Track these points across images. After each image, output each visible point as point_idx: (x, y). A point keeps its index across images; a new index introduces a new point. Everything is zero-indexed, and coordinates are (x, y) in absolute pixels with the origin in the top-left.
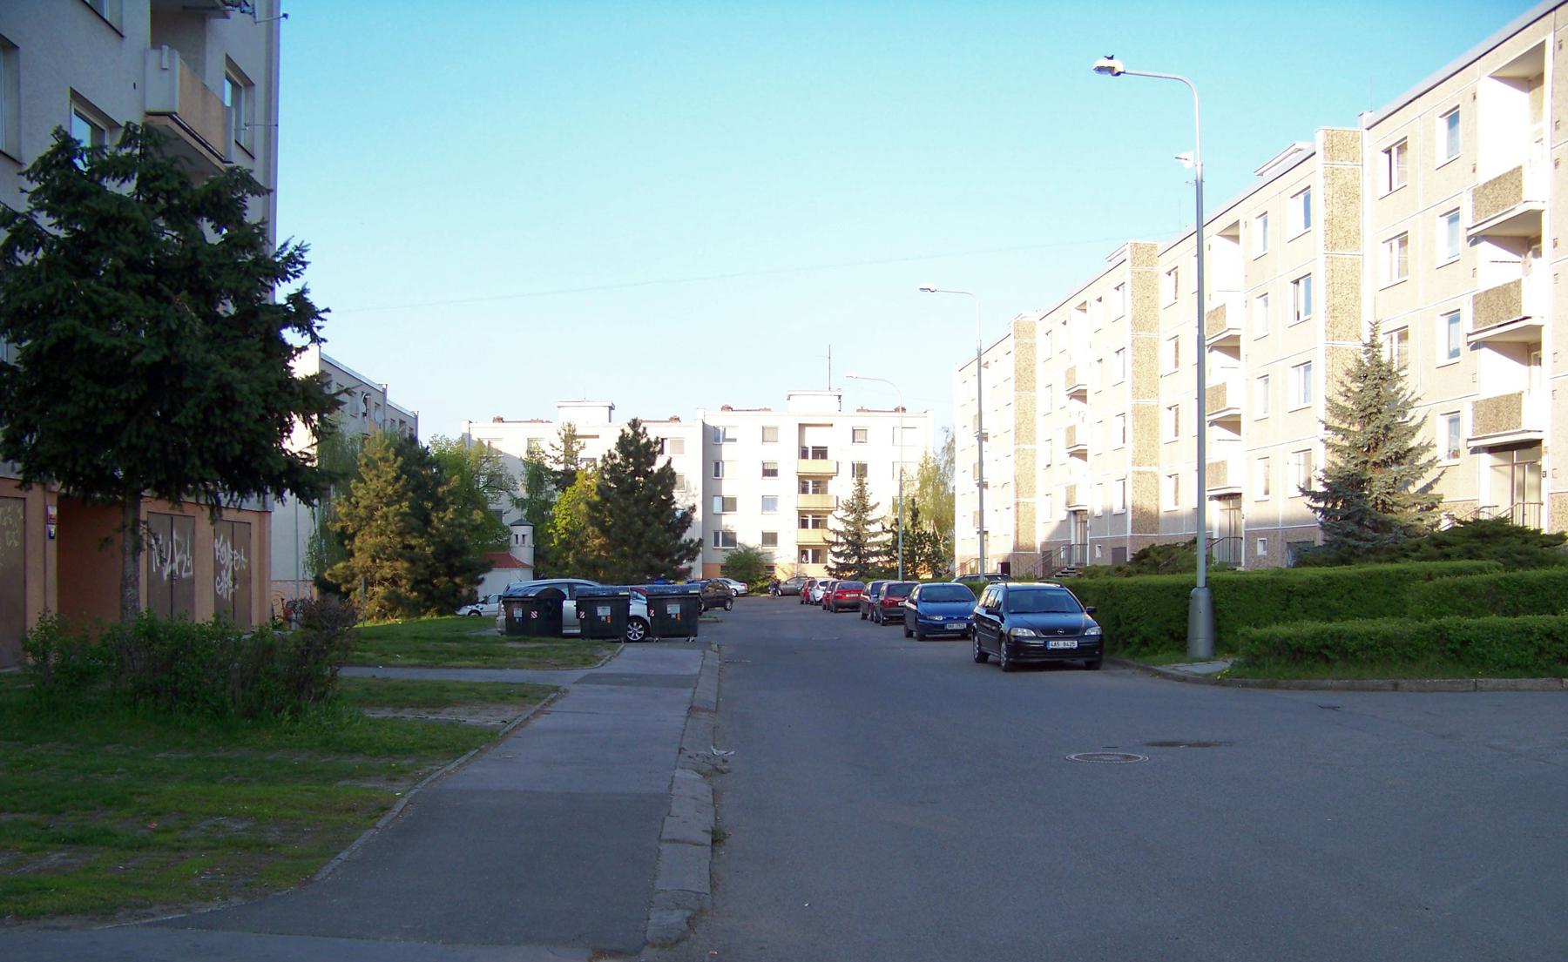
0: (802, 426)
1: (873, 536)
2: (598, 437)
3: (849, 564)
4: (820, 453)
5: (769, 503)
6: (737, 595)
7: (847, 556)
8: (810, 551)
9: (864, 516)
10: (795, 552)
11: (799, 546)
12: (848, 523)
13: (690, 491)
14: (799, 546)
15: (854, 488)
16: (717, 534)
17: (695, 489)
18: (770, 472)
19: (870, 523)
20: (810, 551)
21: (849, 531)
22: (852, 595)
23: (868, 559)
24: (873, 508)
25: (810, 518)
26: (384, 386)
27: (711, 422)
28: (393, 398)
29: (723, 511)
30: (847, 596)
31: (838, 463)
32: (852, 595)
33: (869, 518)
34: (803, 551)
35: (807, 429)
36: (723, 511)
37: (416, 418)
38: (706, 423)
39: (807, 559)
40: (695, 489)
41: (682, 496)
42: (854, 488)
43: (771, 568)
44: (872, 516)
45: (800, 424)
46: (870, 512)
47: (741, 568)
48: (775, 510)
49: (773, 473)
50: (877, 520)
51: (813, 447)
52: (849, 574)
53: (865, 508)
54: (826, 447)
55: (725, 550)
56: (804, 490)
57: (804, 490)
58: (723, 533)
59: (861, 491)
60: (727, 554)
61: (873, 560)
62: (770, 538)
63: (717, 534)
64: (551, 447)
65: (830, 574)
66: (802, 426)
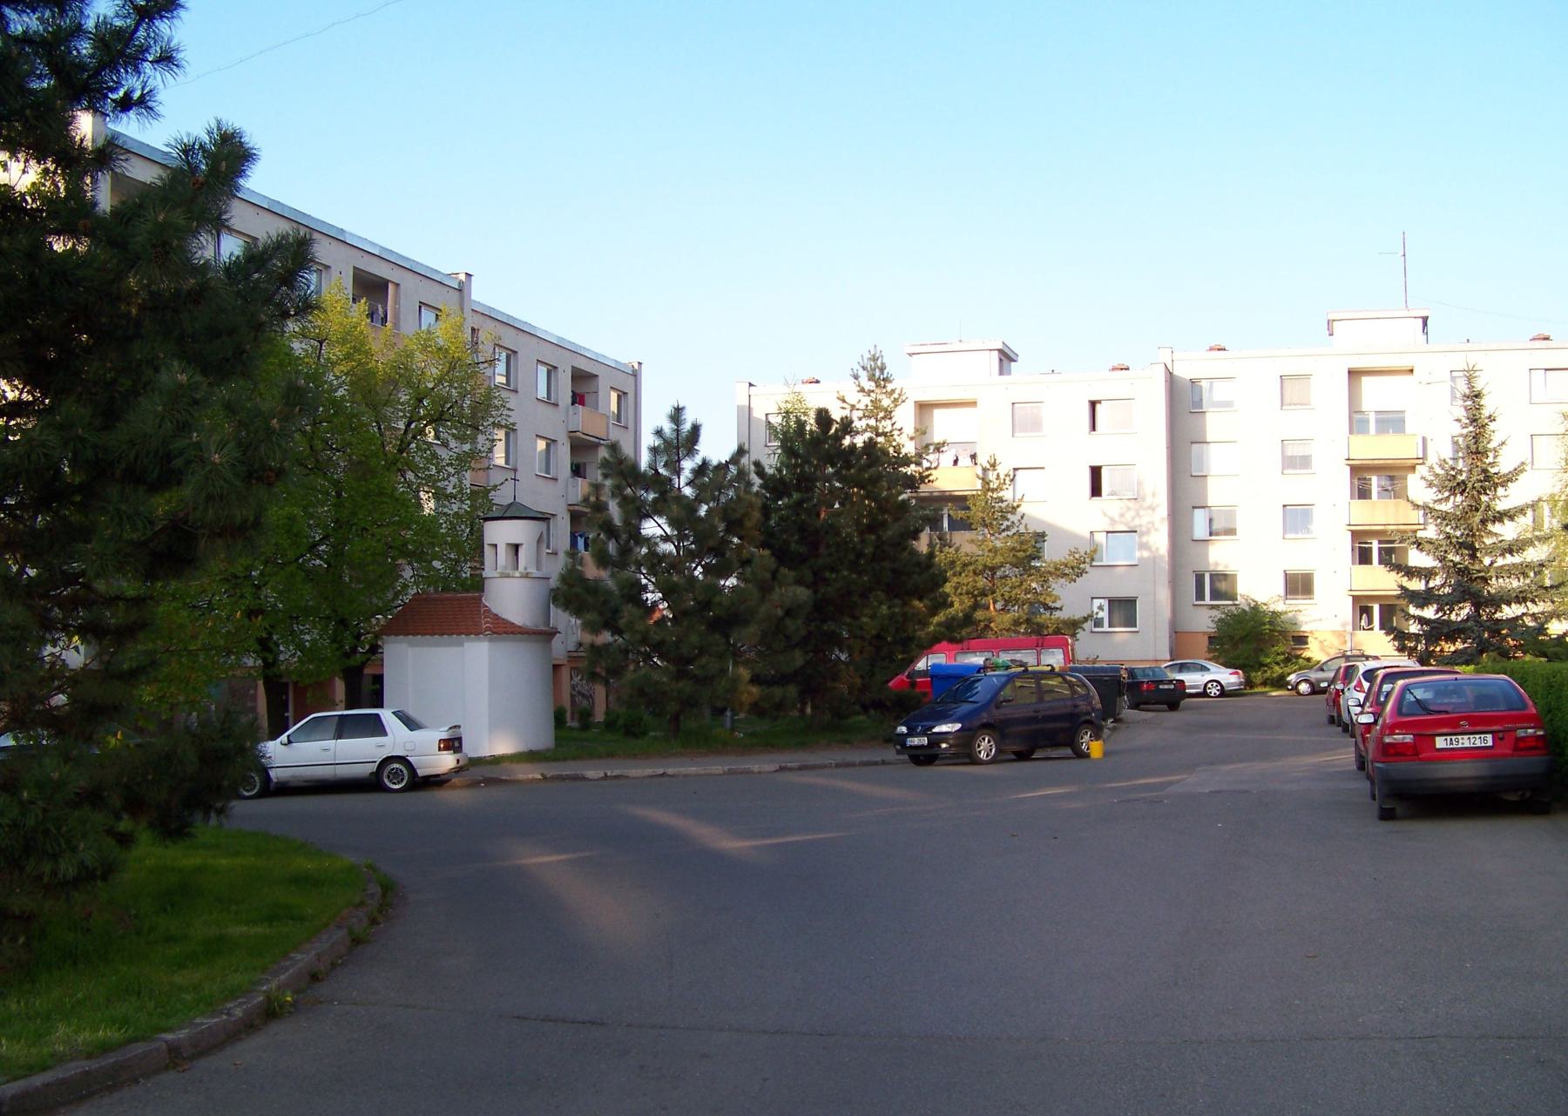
0: (1354, 374)
1: (1511, 551)
2: (973, 404)
3: (1449, 622)
4: (1392, 422)
5: (1296, 517)
6: (1224, 693)
7: (1446, 603)
8: (1376, 609)
9: (1484, 498)
10: (1346, 610)
11: (1354, 598)
12: (1444, 517)
13: (1144, 499)
14: (1354, 598)
15: (1457, 429)
16: (1200, 579)
17: (1154, 495)
18: (1296, 463)
19: (1500, 517)
20: (1376, 609)
21: (1448, 537)
22: (1465, 742)
23: (1498, 608)
24: (1508, 479)
25: (1375, 546)
26: (462, 277)
27: (1183, 372)
28: (481, 294)
29: (1211, 534)
30: (1440, 743)
31: (1424, 440)
32: (1465, 742)
33: (1501, 506)
34: (1362, 607)
35: (1365, 380)
36: (1211, 534)
37: (635, 375)
38: (1175, 373)
39: (1370, 621)
40: (1154, 495)
41: (1129, 509)
42: (1457, 429)
43: (1301, 640)
44: (1506, 499)
45: (1349, 372)
46: (1500, 491)
47: (1243, 639)
48: (1309, 531)
49: (1304, 462)
50: (1521, 511)
51: (1377, 412)
52: (1449, 648)
53: (1490, 481)
54: (1404, 412)
55: (1213, 607)
56: (1363, 493)
57: (1363, 493)
58: (1211, 575)
59: (1477, 438)
60: (1217, 614)
61: (1508, 612)
62: (1299, 585)
63: (1200, 579)
64: (840, 404)
65: (1401, 649)
66: (1354, 374)
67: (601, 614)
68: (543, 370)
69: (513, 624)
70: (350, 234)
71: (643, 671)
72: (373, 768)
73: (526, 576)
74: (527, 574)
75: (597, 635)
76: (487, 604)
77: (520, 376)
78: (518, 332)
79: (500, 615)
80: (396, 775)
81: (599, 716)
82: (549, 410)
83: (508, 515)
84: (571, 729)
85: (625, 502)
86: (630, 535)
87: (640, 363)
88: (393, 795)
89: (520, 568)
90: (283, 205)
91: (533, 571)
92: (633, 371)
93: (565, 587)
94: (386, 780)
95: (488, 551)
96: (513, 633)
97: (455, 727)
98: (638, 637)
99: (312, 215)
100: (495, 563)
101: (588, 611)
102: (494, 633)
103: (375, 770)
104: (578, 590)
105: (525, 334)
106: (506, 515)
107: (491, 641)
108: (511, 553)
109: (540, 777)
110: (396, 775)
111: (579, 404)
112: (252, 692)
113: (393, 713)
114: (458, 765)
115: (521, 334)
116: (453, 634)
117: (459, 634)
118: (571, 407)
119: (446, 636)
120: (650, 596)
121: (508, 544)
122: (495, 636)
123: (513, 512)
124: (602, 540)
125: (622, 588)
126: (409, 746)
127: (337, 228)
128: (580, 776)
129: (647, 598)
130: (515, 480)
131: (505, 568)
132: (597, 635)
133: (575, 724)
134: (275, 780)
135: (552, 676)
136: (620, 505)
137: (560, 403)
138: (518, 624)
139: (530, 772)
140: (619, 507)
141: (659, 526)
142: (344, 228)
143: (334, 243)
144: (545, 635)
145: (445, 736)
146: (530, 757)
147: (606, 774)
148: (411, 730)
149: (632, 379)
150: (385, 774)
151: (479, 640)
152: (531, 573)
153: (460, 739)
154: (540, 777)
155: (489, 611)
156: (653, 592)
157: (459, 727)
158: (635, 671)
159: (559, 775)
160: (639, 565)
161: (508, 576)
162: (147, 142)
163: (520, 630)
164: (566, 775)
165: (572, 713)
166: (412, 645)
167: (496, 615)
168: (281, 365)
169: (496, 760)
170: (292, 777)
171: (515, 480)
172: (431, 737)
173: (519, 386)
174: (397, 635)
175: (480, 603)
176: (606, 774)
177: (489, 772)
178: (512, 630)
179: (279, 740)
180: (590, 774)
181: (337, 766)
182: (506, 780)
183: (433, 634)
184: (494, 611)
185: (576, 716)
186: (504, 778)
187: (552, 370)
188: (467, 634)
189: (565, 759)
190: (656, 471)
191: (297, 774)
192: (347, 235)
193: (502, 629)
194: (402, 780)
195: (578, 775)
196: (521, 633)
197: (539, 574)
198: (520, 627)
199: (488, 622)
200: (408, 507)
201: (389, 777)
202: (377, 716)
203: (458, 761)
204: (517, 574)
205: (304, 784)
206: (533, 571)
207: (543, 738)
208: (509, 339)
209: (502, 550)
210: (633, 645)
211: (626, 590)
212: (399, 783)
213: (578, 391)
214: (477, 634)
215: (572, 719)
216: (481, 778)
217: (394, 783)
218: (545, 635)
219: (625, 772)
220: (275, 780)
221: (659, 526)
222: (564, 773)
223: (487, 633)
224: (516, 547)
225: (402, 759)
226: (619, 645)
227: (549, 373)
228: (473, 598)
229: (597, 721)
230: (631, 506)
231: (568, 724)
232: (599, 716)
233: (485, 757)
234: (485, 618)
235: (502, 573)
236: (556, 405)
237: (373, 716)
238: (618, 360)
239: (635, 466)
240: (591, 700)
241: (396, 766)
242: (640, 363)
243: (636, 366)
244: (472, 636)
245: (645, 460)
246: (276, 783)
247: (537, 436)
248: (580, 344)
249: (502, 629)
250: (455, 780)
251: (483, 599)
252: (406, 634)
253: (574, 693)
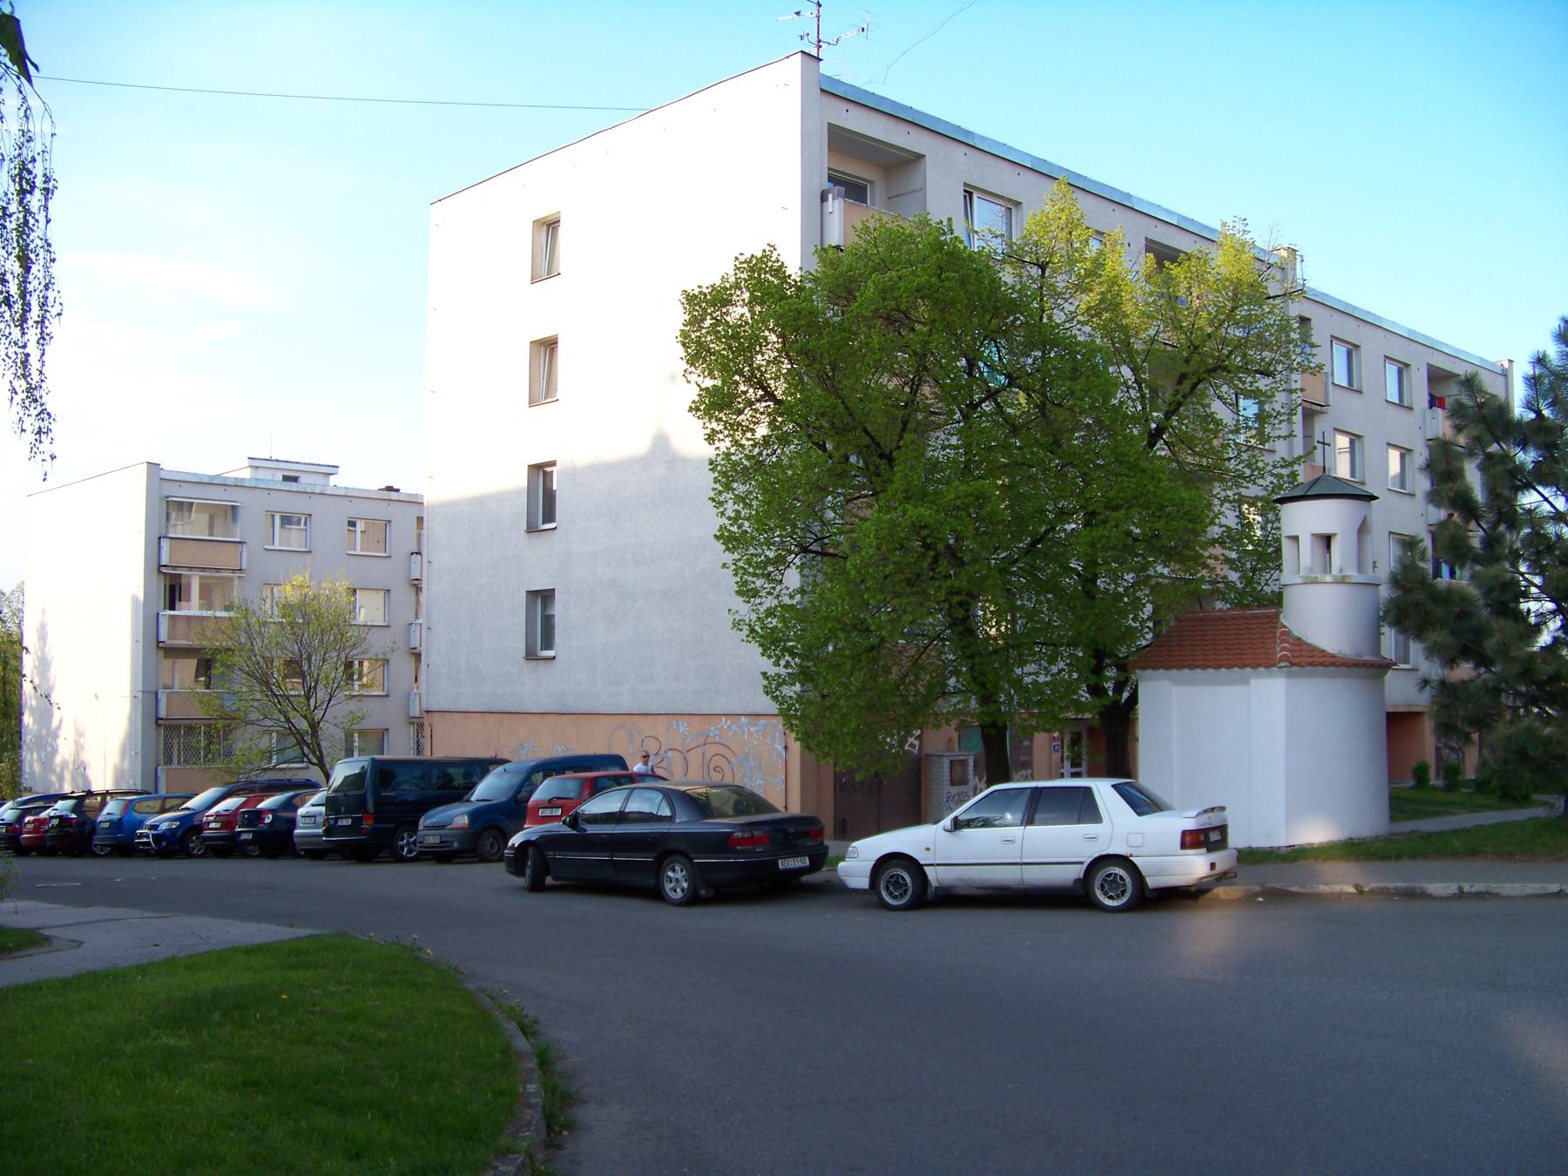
67: (1454, 633)
68: (1392, 371)
69: (1324, 651)
70: (1139, 199)
71: (1525, 722)
72: (1078, 872)
73: (1342, 581)
74: (1344, 577)
75: (1452, 669)
76: (1285, 624)
77: (1364, 373)
78: (1361, 324)
79: (1304, 639)
80: (1113, 884)
81: (1470, 774)
82: (1401, 413)
83: (1314, 493)
84: (1434, 788)
85: (1490, 464)
86: (1500, 513)
87: (1511, 361)
88: (1104, 915)
89: (1333, 569)
90: (1051, 163)
91: (1353, 574)
92: (1503, 370)
93: (1399, 593)
94: (1098, 893)
95: (1287, 547)
96: (1321, 664)
97: (1212, 809)
98: (1516, 669)
99: (1089, 176)
100: (1299, 559)
101: (1434, 630)
102: (1293, 664)
103: (1081, 876)
104: (1420, 596)
105: (1369, 326)
106: (1309, 493)
107: (1289, 676)
108: (1320, 546)
109: (1352, 890)
110: (1113, 884)
111: (1439, 407)
112: (1026, 743)
113: (1113, 786)
114: (1213, 872)
115: (1363, 326)
116: (1259, 666)
117: (1242, 666)
118: (1428, 412)
119: (1223, 670)
120: (1533, 606)
121: (1315, 536)
122: (1295, 669)
123: (1324, 489)
124: (1455, 523)
125: (1488, 592)
126: (1136, 840)
127: (1122, 192)
128: (1418, 891)
129: (1529, 610)
130: (1324, 443)
131: (1311, 570)
132: (1452, 669)
133: (1439, 783)
134: (934, 883)
135: (1384, 730)
136: (1482, 468)
137: (1415, 406)
138: (1331, 652)
139: (1342, 880)
140: (1480, 470)
141: (1546, 499)
142: (1131, 193)
143: (1118, 209)
144: (1373, 668)
145: (1191, 825)
146: (1352, 850)
147: (1461, 889)
148: (1139, 814)
149: (1501, 379)
150: (1097, 883)
151: (1271, 676)
152: (1349, 576)
153: (1222, 829)
154: (1352, 890)
155: (1288, 633)
156: (1537, 599)
157: (1223, 809)
158: (1511, 722)
159: (1386, 888)
160: (1515, 557)
161: (1314, 582)
162: (872, 91)
163: (1333, 660)
164: (1395, 888)
165: (1438, 769)
166: (1176, 682)
167: (1299, 639)
168: (963, 282)
169: (1296, 855)
170: (959, 880)
171: (1324, 443)
172: (1168, 827)
173: (1364, 386)
174: (1155, 668)
175: (1277, 623)
176: (1461, 889)
177: (1272, 877)
178: (1322, 660)
179: (941, 824)
180: (1435, 888)
181: (1024, 867)
182: (1298, 894)
183: (1205, 667)
184: (1296, 633)
185: (1442, 773)
186: (1294, 889)
187: (1403, 368)
188: (1255, 666)
189: (1398, 857)
190: (1538, 413)
191: (966, 877)
192: (1135, 201)
193: (1306, 659)
194: (1123, 892)
195: (1413, 889)
196: (1333, 664)
197: (1362, 579)
198: (1333, 656)
199: (1283, 649)
200: (1160, 480)
201: (1102, 887)
202: (1088, 790)
203: (1213, 866)
204: (1328, 578)
205: (982, 892)
206: (1353, 574)
207: (1369, 821)
208: (1350, 331)
209: (1306, 543)
210: (1507, 683)
211: (1495, 595)
212: (1118, 897)
213: (1437, 394)
214: (1268, 666)
215: (1438, 775)
216: (1258, 889)
217: (1111, 898)
218: (1373, 668)
219: (1494, 887)
220: (934, 883)
221: (1546, 499)
222: (1392, 885)
223: (1282, 664)
224: (1327, 540)
225: (1124, 861)
226: (1485, 681)
227: (1400, 372)
228: (1266, 616)
229: (1468, 778)
230: (1499, 469)
231: (1432, 783)
232: (1470, 774)
233: (1279, 848)
234: (1281, 643)
235: (1307, 577)
236: (1410, 408)
237: (1083, 790)
238: (1483, 357)
239: (1504, 409)
240: (1460, 753)
241: (1120, 871)
242: (1511, 361)
243: (1506, 365)
244: (1262, 669)
245: (1519, 411)
246: (936, 888)
247: (1389, 444)
248: (1438, 339)
249: (1306, 659)
250: (1221, 891)
251: (1281, 616)
252: (1168, 667)
253: (1440, 745)
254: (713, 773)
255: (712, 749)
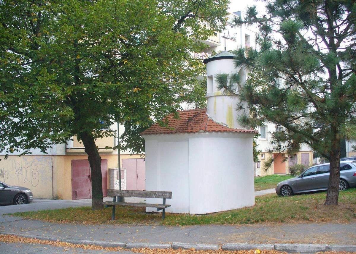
163: (225, 130)
254: (33, 175)
255: (33, 167)
